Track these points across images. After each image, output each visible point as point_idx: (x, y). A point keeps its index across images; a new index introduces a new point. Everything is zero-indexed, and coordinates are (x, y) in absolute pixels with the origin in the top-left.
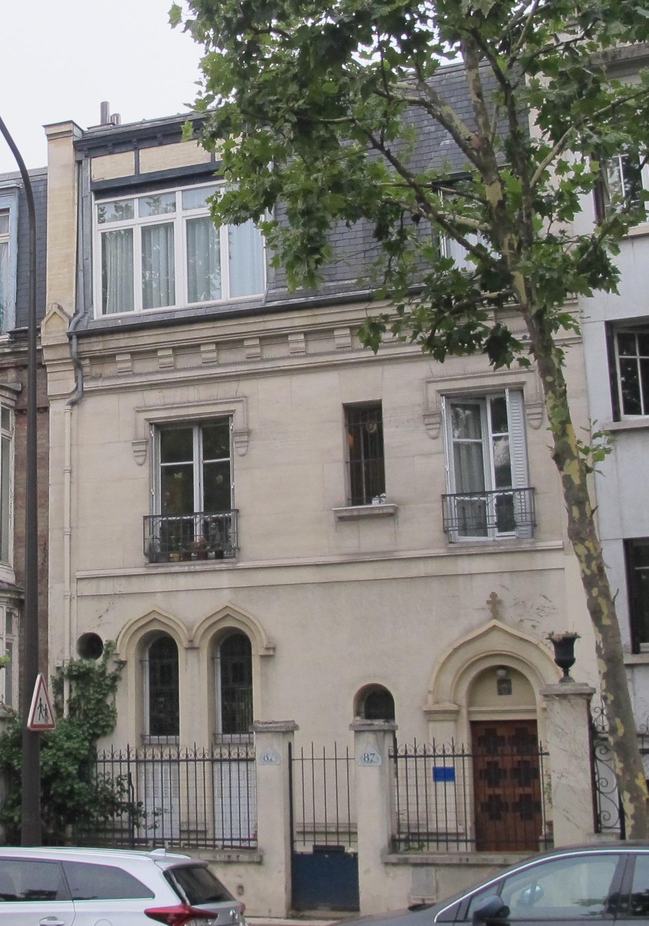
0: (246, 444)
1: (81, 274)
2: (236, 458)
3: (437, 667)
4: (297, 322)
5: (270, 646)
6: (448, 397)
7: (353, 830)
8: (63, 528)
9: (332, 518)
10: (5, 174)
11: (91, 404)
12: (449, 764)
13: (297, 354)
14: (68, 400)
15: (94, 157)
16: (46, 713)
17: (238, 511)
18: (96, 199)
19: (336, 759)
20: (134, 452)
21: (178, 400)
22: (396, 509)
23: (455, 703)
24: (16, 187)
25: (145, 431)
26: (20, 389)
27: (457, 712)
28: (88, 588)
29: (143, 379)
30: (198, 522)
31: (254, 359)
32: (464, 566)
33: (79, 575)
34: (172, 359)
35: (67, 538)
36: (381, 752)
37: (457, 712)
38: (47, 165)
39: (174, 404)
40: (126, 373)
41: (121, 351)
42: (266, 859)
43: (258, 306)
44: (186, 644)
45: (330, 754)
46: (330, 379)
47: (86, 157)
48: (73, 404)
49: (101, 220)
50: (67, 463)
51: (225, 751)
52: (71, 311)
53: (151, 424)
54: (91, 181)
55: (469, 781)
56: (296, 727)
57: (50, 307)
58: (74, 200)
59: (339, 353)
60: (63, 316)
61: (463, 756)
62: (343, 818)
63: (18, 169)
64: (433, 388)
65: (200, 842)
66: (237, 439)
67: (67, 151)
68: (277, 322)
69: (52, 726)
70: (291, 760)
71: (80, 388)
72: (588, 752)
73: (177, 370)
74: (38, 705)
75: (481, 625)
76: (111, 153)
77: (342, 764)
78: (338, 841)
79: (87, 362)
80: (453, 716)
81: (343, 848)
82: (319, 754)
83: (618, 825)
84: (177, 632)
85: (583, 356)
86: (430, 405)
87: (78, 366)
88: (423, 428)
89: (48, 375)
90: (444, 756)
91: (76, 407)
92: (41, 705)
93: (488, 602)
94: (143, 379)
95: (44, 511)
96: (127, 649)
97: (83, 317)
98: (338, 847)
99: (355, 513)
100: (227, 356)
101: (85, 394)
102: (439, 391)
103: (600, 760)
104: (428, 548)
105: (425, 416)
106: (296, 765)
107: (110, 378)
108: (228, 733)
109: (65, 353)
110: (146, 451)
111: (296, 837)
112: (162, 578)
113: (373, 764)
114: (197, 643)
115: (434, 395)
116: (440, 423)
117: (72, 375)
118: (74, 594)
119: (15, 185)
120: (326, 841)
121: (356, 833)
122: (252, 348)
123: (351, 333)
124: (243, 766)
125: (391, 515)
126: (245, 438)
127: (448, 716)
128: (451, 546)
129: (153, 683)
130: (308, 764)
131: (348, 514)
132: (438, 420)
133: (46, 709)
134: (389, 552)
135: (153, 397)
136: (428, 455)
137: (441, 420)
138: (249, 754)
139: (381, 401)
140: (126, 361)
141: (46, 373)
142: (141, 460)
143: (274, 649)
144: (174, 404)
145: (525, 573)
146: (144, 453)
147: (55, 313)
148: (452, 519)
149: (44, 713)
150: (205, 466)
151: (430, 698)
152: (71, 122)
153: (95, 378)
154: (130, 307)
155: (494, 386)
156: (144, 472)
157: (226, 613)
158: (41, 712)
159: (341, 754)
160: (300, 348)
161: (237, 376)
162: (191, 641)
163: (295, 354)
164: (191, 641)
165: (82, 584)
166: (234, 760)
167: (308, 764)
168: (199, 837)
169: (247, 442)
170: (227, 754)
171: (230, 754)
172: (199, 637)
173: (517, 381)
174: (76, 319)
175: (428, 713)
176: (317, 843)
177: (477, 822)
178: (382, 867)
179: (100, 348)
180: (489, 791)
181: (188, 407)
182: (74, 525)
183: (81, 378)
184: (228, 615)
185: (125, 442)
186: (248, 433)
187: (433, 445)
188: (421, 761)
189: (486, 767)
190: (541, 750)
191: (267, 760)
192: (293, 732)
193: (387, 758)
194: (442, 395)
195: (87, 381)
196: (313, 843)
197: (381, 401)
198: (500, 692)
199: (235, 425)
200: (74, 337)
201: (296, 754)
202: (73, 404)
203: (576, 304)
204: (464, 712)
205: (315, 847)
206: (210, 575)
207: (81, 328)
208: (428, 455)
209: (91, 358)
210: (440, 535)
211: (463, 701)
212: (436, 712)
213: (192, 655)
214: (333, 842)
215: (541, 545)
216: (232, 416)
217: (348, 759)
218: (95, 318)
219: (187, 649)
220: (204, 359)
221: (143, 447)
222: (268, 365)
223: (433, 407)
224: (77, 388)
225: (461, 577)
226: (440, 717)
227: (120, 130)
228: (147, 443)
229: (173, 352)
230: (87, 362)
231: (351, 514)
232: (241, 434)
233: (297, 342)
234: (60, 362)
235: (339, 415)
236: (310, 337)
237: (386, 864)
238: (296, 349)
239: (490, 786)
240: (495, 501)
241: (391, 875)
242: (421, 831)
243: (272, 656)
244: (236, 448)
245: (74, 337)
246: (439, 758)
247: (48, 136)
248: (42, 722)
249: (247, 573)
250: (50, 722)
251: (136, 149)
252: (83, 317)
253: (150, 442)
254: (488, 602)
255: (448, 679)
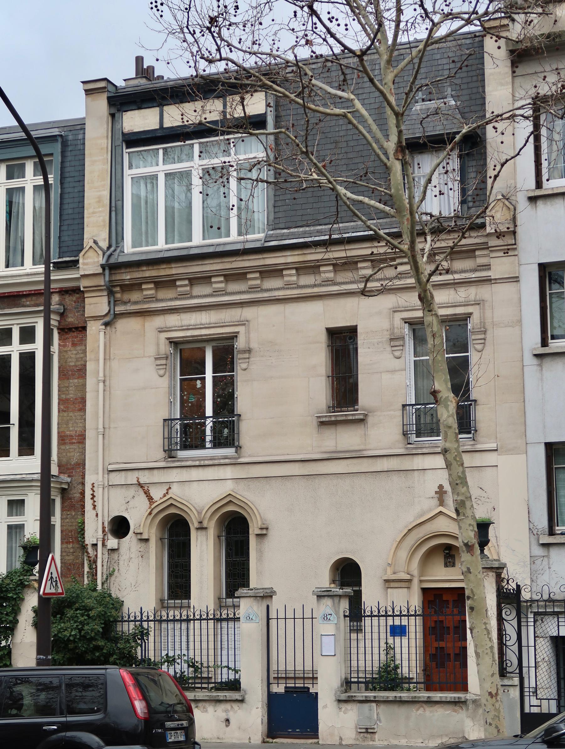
0: (247, 360)
1: (113, 214)
2: (240, 372)
3: (395, 545)
4: (290, 260)
5: (264, 526)
6: (410, 324)
7: (315, 676)
8: (97, 429)
9: (315, 422)
10: (50, 123)
11: (122, 325)
12: (405, 622)
13: (289, 286)
14: (102, 322)
15: (125, 111)
16: (56, 584)
17: (240, 415)
18: (127, 148)
19: (285, 619)
20: (157, 365)
21: (192, 322)
22: (366, 415)
23: (408, 574)
24: (59, 135)
25: (165, 348)
26: (62, 311)
27: (410, 581)
28: (117, 479)
29: (463, 275)
30: (209, 424)
31: (219, 293)
32: (419, 462)
33: (111, 467)
34: (188, 288)
35: (101, 437)
36: (337, 613)
37: (410, 581)
38: (83, 115)
39: (189, 326)
40: (149, 299)
41: (147, 280)
42: (247, 697)
43: (258, 245)
44: (196, 525)
45: (299, 614)
46: (316, 307)
47: (119, 110)
48: (106, 324)
49: (130, 167)
50: (101, 374)
51: (177, 613)
52: (104, 244)
53: (171, 342)
54: (122, 133)
55: (420, 635)
56: (274, 593)
57: (88, 242)
58: (107, 148)
59: (323, 286)
60: (97, 249)
61: (415, 615)
62: (308, 667)
63: (16, 124)
64: (398, 317)
65: (197, 685)
66: (240, 356)
67: (101, 103)
68: (273, 259)
69: (62, 594)
70: (268, 619)
71: (112, 312)
72: (496, 613)
73: (192, 297)
74: (49, 578)
75: (431, 510)
76: (140, 108)
77: (308, 622)
78: (304, 684)
79: (118, 289)
80: (406, 584)
81: (309, 688)
82: (290, 615)
83: (517, 671)
84: (189, 515)
85: (519, 292)
86: (396, 330)
87: (111, 293)
88: (389, 349)
89: (86, 300)
90: (400, 616)
91: (108, 328)
92: (52, 578)
93: (436, 492)
94: (463, 275)
95: (82, 414)
96: (149, 530)
97: (115, 250)
98: (304, 687)
99: (333, 419)
100: (233, 287)
101: (117, 316)
102: (403, 319)
103: (505, 620)
104: (390, 448)
105: (391, 340)
106: (273, 623)
107: (136, 303)
108: (172, 599)
109: (101, 281)
110: (166, 365)
111: (272, 680)
112: (178, 470)
113: (330, 622)
114: (205, 524)
115: (399, 322)
116: (403, 346)
117: (105, 300)
118: (106, 484)
119: (58, 133)
120: (304, 684)
121: (317, 678)
122: (254, 280)
123: (372, 265)
124: (231, 624)
125: (362, 421)
126: (247, 355)
127: (403, 584)
128: (409, 446)
129: (170, 556)
130: (282, 622)
131: (327, 419)
132: (401, 343)
133: (56, 581)
134: (360, 451)
135: (172, 320)
136: (393, 371)
137: (404, 343)
138: (236, 614)
139: (357, 326)
140: (221, 282)
141: (84, 298)
142: (162, 372)
143: (267, 529)
144: (189, 326)
145: (331, 476)
146: (164, 367)
147: (91, 247)
148: (413, 424)
149: (54, 584)
150: (213, 377)
151: (389, 571)
152: (105, 79)
153: (125, 303)
154: (155, 243)
155: (447, 315)
156: (164, 383)
157: (230, 499)
158: (52, 583)
159: (308, 614)
160: (293, 281)
161: (241, 303)
162: (201, 522)
163: (288, 286)
164: (201, 522)
165: (113, 475)
166: (171, 620)
167: (282, 622)
168: (197, 681)
169: (249, 358)
170: (166, 615)
171: (221, 615)
172: (207, 519)
173: (466, 312)
174: (109, 253)
175: (387, 581)
176: (288, 685)
177: (426, 669)
178: (336, 703)
179: (128, 277)
180: (436, 645)
181: (201, 328)
182: (107, 426)
183: (113, 301)
184: (231, 501)
185: (149, 357)
186: (249, 351)
187: (397, 364)
188: (382, 619)
189: (433, 625)
190: (365, 612)
191: (249, 619)
192: (271, 597)
193: (342, 617)
194: (406, 323)
195: (118, 305)
196: (285, 685)
197: (357, 326)
198: (446, 566)
199: (240, 344)
200: (107, 268)
201: (273, 615)
202: (106, 324)
203: (516, 249)
204: (416, 582)
205: (286, 687)
206: (216, 468)
207: (112, 261)
208: (393, 371)
209: (121, 286)
210: (400, 437)
211: (416, 573)
212: (394, 581)
213: (201, 533)
214: (299, 684)
215: (479, 447)
216: (236, 336)
217: (285, 619)
218: (126, 251)
219: (197, 529)
220: (215, 288)
221: (164, 362)
222: (266, 295)
223: (397, 332)
224: (109, 311)
225: (416, 472)
226: (396, 585)
227: (159, 85)
228: (167, 358)
229: (334, 267)
230: (118, 289)
231: (330, 419)
232: (244, 352)
233: (290, 275)
234: (96, 289)
235: (323, 337)
236: (301, 272)
237: (339, 701)
238: (289, 281)
239: (436, 640)
240: (211, 424)
241: (343, 709)
242: (203, 676)
243: (265, 534)
244: (240, 365)
245: (107, 268)
246: (132, 623)
247: (86, 91)
248: (53, 591)
249: (247, 467)
250: (60, 590)
251: (161, 105)
252: (115, 250)
253: (170, 357)
254: (436, 492)
255: (403, 554)
